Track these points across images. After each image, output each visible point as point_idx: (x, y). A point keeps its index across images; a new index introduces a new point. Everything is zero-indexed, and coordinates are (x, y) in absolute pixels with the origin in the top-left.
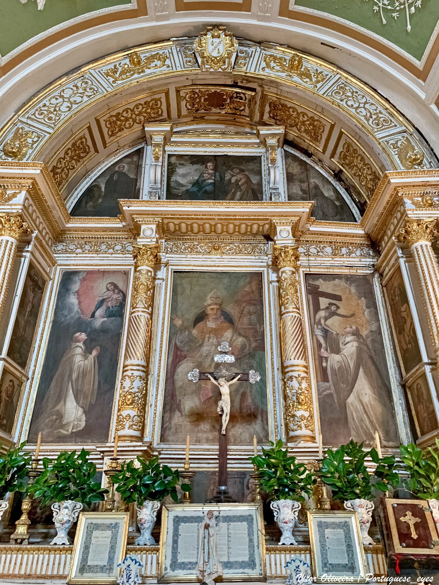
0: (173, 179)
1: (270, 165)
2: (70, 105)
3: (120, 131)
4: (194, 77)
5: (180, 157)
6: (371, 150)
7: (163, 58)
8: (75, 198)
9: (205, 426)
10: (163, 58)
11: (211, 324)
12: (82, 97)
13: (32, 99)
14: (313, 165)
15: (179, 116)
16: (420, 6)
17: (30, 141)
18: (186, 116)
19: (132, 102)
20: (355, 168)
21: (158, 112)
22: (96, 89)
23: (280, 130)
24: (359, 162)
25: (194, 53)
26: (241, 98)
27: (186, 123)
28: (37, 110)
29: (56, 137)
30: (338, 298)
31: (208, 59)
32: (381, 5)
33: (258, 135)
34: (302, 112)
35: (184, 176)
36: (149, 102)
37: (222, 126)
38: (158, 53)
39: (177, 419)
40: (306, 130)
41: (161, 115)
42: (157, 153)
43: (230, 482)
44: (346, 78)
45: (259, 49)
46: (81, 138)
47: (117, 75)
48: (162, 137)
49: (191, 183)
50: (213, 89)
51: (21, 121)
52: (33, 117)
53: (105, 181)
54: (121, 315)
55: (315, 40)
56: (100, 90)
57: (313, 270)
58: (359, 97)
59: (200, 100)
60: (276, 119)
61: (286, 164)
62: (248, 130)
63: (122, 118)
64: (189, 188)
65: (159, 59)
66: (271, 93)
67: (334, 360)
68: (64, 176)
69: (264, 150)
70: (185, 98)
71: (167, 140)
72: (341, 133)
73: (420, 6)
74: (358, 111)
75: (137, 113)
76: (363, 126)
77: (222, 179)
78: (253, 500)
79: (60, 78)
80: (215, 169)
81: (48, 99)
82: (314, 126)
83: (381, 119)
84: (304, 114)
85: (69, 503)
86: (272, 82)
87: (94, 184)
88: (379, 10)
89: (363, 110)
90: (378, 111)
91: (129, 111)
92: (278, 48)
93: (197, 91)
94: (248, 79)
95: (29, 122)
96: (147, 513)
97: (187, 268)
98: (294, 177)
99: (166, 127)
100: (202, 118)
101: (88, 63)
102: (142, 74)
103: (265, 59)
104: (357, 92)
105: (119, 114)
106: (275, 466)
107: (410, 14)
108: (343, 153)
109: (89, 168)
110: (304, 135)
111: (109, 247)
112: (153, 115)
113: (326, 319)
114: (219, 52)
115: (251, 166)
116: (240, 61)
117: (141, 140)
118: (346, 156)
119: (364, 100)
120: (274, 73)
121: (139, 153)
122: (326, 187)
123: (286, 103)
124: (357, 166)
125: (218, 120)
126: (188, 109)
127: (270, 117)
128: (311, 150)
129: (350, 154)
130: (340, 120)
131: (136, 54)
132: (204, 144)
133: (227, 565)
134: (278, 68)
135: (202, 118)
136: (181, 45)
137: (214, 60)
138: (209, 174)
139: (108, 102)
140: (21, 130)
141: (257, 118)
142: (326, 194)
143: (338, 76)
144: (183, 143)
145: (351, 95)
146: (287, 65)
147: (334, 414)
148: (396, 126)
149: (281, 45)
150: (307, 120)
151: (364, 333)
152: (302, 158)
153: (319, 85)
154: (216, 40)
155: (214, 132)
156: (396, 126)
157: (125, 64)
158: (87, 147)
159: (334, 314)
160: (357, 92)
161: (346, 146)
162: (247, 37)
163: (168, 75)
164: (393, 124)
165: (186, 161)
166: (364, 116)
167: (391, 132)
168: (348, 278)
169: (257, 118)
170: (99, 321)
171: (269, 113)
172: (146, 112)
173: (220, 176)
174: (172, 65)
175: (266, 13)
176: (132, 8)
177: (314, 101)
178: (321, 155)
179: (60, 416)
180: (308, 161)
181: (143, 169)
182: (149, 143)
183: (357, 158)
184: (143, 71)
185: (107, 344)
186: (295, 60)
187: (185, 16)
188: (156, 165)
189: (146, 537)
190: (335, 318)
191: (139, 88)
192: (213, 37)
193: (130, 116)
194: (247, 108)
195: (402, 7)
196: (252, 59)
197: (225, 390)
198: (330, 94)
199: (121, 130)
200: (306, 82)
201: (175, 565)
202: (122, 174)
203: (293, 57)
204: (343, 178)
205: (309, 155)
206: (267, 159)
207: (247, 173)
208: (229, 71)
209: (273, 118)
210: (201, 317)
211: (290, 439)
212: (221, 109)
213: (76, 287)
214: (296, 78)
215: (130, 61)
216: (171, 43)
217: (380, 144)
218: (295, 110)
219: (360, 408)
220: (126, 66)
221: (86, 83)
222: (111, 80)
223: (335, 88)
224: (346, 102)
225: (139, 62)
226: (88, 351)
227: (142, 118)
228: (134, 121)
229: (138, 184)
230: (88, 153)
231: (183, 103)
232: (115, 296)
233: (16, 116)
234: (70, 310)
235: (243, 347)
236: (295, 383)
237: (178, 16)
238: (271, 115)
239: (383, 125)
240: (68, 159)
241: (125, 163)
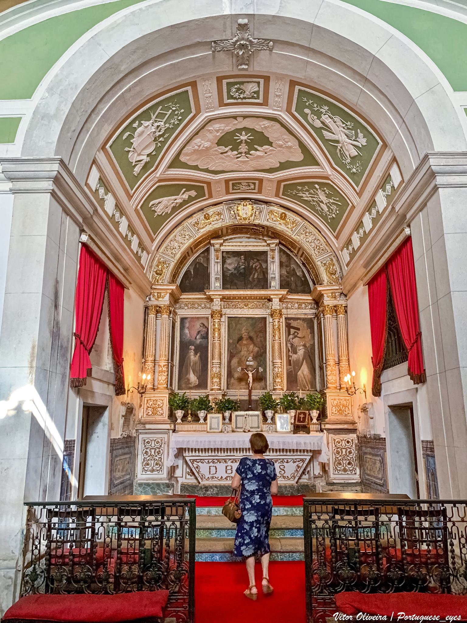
0: (225, 266)
5: (228, 252)
9: (243, 383)
11: (245, 342)
23: (277, 241)
30: (298, 329)
35: (230, 264)
39: (232, 380)
43: (252, 403)
54: (207, 338)
57: (289, 316)
67: (294, 357)
72: (303, 253)
77: (249, 264)
78: (260, 410)
85: (203, 411)
96: (227, 414)
97: (233, 316)
106: (266, 400)
111: (199, 305)
113: (293, 339)
115: (263, 257)
121: (207, 251)
133: (251, 428)
142: (298, 274)
147: (292, 379)
151: (308, 345)
153: (293, 229)
159: (296, 337)
165: (231, 255)
168: (304, 320)
170: (198, 341)
179: (189, 380)
180: (291, 254)
185: (203, 350)
189: (227, 420)
190: (297, 338)
197: (250, 375)
201: (236, 428)
210: (240, 339)
211: (274, 389)
213: (187, 325)
219: (303, 376)
226: (196, 354)
232: (204, 329)
234: (186, 336)
235: (258, 352)
236: (276, 369)
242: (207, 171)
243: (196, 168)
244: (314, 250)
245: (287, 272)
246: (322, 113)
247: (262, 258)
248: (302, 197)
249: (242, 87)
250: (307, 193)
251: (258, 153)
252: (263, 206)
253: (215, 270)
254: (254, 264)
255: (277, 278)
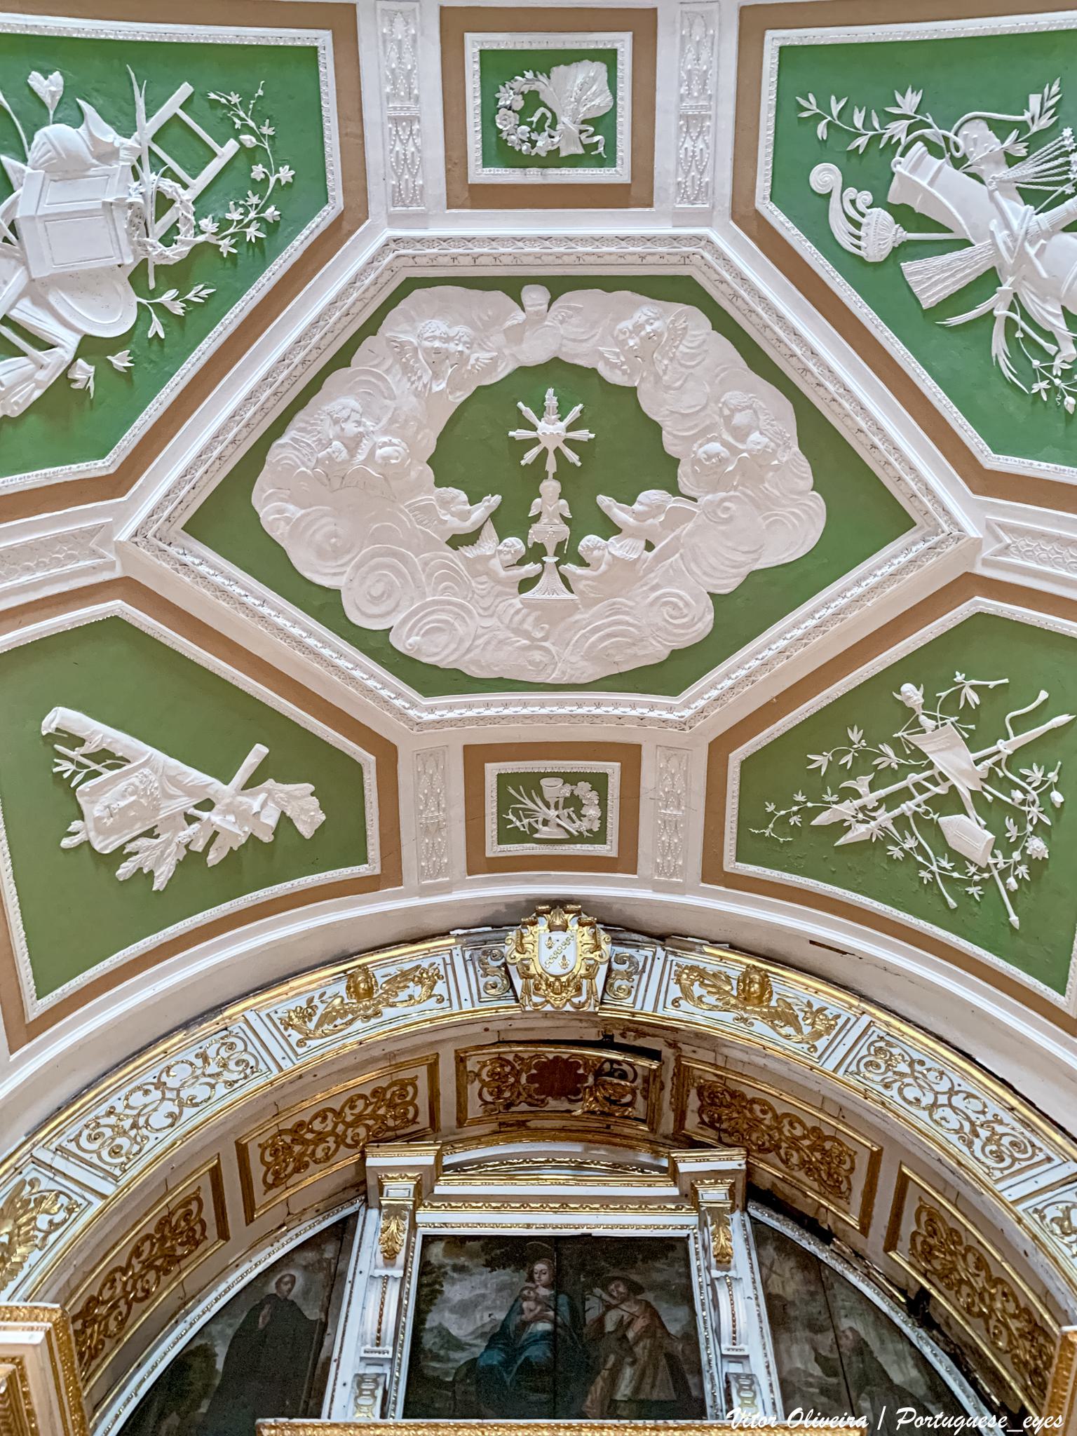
0: (432, 1320)
1: (716, 1273)
2: (176, 1110)
3: (297, 1170)
4: (502, 1025)
5: (458, 1243)
6: (998, 1235)
7: (426, 978)
8: (129, 1400)
10: (426, 978)
12: (213, 1087)
13: (84, 1096)
14: (840, 1267)
15: (461, 1122)
16: (1027, 877)
17: (43, 1222)
18: (478, 1122)
19: (335, 1093)
20: (965, 1290)
21: (405, 1114)
22: (252, 1063)
23: (734, 1161)
24: (972, 1270)
25: (505, 965)
26: (624, 1076)
27: (478, 1141)
28: (87, 1126)
29: (119, 1209)
31: (536, 982)
32: (934, 868)
33: (673, 1173)
34: (787, 1115)
36: (385, 1090)
37: (577, 1148)
38: (418, 967)
40: (803, 1163)
41: (414, 1121)
42: (392, 1238)
44: (888, 1024)
45: (661, 953)
46: (187, 1202)
47: (311, 1025)
48: (411, 1185)
49: (483, 1335)
50: (550, 1052)
51: (37, 1162)
52: (72, 1147)
53: (230, 1332)
55: (796, 935)
56: (262, 1066)
58: (932, 1076)
59: (518, 1081)
60: (719, 1130)
61: (761, 1264)
62: (645, 1158)
63: (309, 1136)
64: (477, 1352)
65: (421, 982)
66: (702, 1067)
68: (113, 1326)
69: (692, 1219)
70: (478, 1075)
71: (423, 1193)
72: (903, 1180)
73: (1027, 877)
74: (936, 1117)
75: (349, 1119)
76: (959, 1163)
77: (577, 1314)
79: (168, 1035)
80: (556, 1284)
81: (120, 1097)
82: (825, 1152)
83: (1006, 1141)
84: (794, 1121)
86: (699, 1036)
87: (198, 1342)
88: (934, 878)
89: (948, 1112)
90: (989, 1117)
91: (330, 1115)
92: (707, 949)
93: (511, 1057)
94: (640, 1029)
95: (59, 1163)
98: (792, 1312)
99: (425, 1158)
100: (522, 1124)
101: (245, 996)
102: (373, 1021)
103: (679, 976)
104: (922, 1063)
105: (301, 1125)
107: (1008, 891)
108: (919, 1240)
109: (190, 1288)
110: (801, 1175)
112: (391, 1123)
114: (565, 965)
115: (661, 1272)
116: (617, 983)
117: (353, 1192)
118: (931, 1248)
119: (944, 1086)
120: (702, 1014)
121: (343, 1232)
122: (890, 1346)
123: (743, 1089)
124: (968, 1283)
125: (563, 1129)
126: (486, 1103)
127: (703, 1122)
128: (827, 1223)
129: (940, 1242)
130: (893, 1141)
131: (366, 971)
132: (524, 1202)
134: (711, 999)
135: (522, 1124)
136: (476, 945)
137: (557, 985)
138: (537, 1301)
139: (274, 1101)
140: (28, 1188)
141: (668, 1123)
142: (897, 1378)
143: (865, 1020)
144: (466, 1200)
145: (907, 1070)
146: (734, 993)
148: (1049, 1159)
149: (713, 942)
150: (804, 1137)
152: (804, 1244)
153: (821, 1044)
154: (559, 936)
155: (552, 1162)
156: (1049, 1159)
157: (336, 996)
158: (198, 1228)
160: (922, 1063)
161: (924, 1217)
162: (629, 925)
163: (438, 1023)
164: (1041, 1156)
165: (472, 1255)
166: (957, 1132)
167: (1044, 1181)
169: (668, 1123)
171: (700, 1111)
172: (373, 1116)
173: (573, 1310)
174: (446, 999)
175: (671, 876)
176: (369, 873)
177: (816, 1088)
178: (857, 1239)
181: (348, 1286)
182: (372, 1202)
183: (964, 1257)
184: (377, 1014)
186: (752, 981)
187: (487, 883)
188: (386, 1279)
191: (366, 1056)
192: (552, 928)
193: (329, 1128)
194: (639, 1097)
195: (986, 875)
196: (645, 976)
198: (853, 1068)
199: (301, 1167)
200: (787, 1037)
202: (284, 1307)
203: (746, 974)
204: (938, 1320)
205: (825, 1237)
206: (705, 1249)
207: (649, 1296)
208: (591, 1009)
209: (711, 1125)
212: (571, 1101)
214: (761, 1027)
215: (348, 988)
216: (453, 941)
217: (1020, 1221)
218: (767, 1108)
220: (337, 1001)
221: (232, 1046)
222: (295, 1036)
223: (864, 1052)
224: (900, 1091)
225: (369, 992)
227: (362, 1131)
228: (340, 1140)
229: (327, 1342)
230: (197, 1244)
231: (473, 1089)
233: (28, 1146)
237: (471, 885)
238: (707, 1120)
239: (1014, 1160)
240: (138, 1268)
241: (297, 1267)
242: (376, 646)
243: (325, 606)
244: (970, 1145)
245: (819, 1359)
246: (892, 147)
247: (658, 1277)
248: (841, 827)
249: (542, 85)
250: (862, 784)
251: (617, 547)
252: (648, 952)
253: (370, 1315)
254: (610, 1310)
255: (763, 1379)
